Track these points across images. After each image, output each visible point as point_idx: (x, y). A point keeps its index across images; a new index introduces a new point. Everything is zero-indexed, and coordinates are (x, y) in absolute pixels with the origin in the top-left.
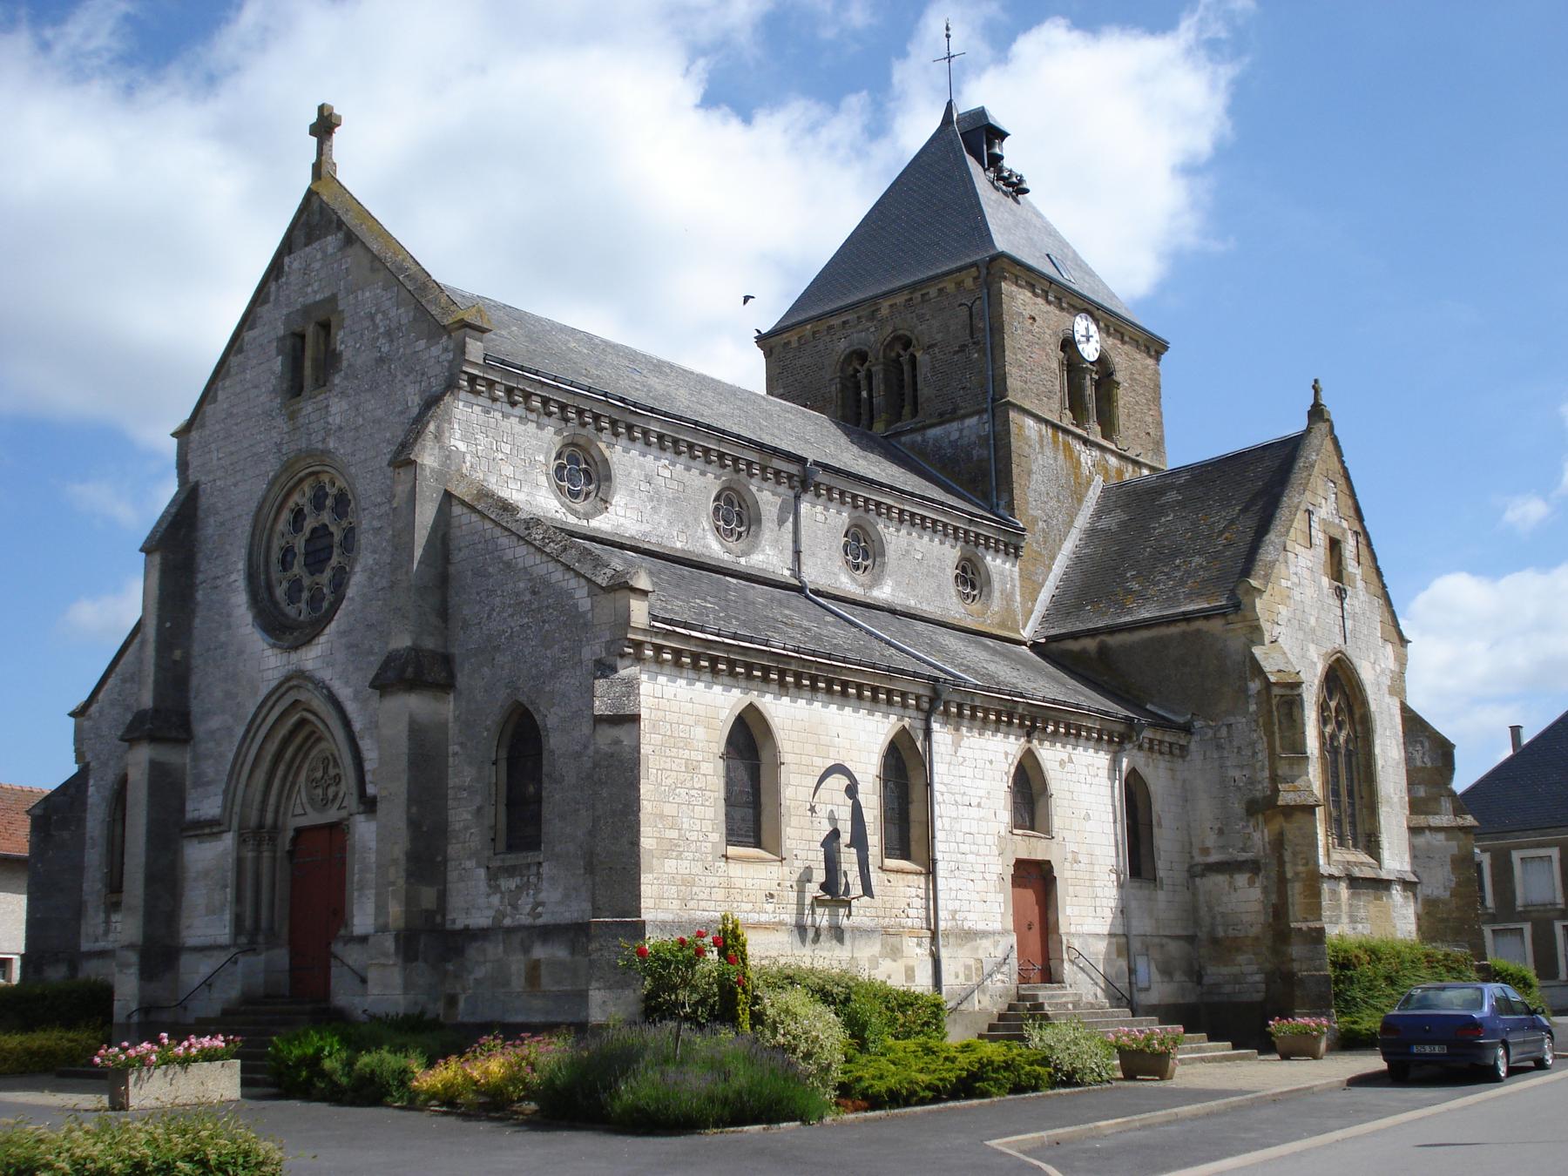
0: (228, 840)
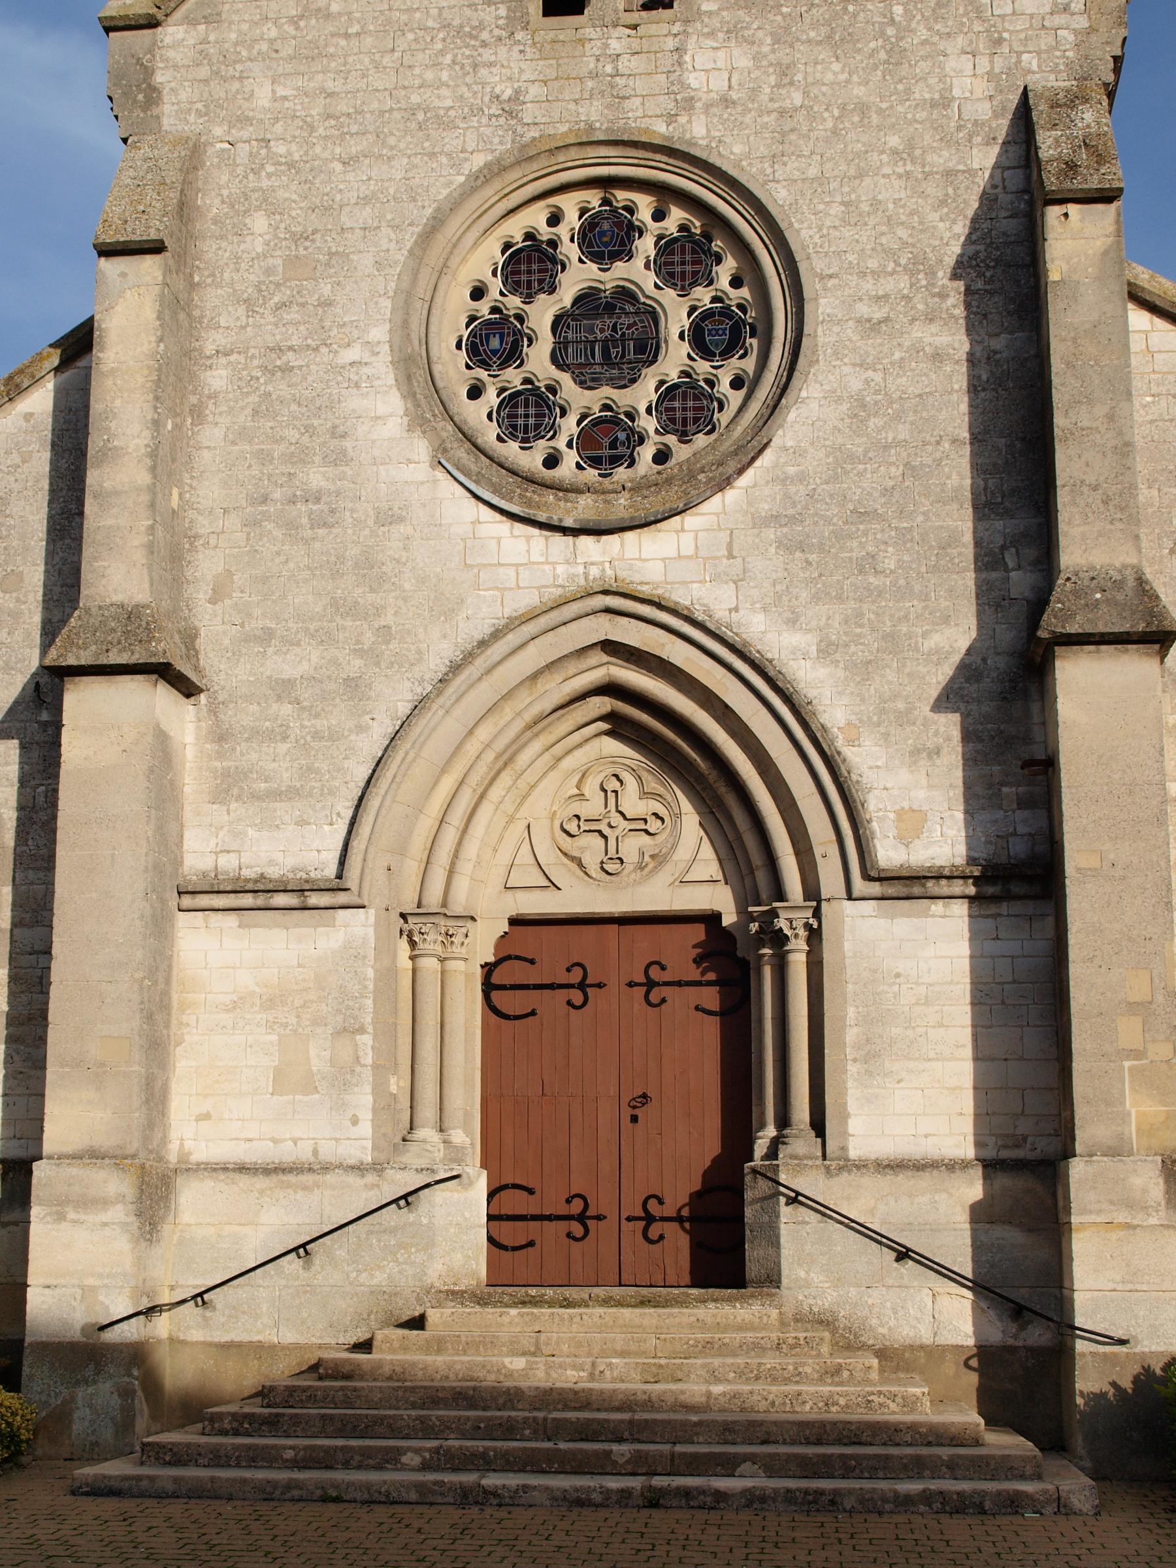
0: (358, 927)
